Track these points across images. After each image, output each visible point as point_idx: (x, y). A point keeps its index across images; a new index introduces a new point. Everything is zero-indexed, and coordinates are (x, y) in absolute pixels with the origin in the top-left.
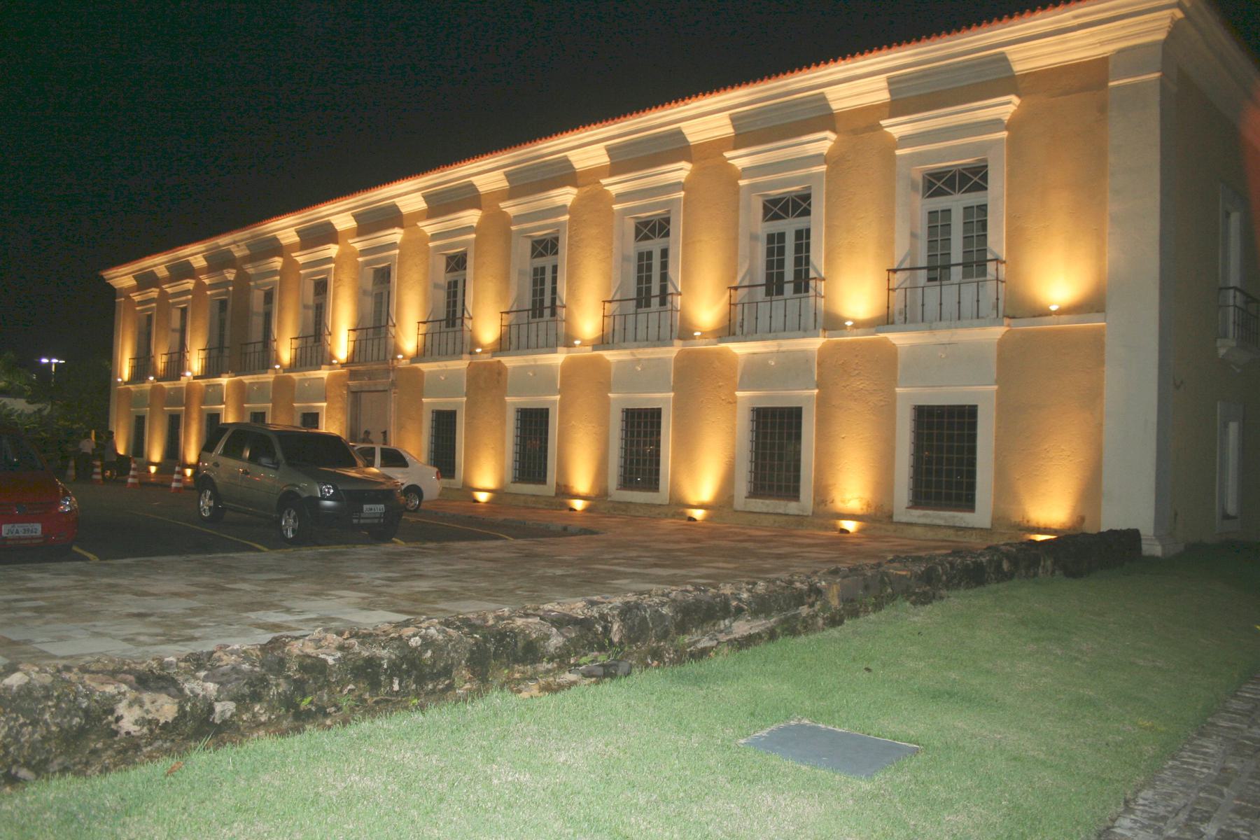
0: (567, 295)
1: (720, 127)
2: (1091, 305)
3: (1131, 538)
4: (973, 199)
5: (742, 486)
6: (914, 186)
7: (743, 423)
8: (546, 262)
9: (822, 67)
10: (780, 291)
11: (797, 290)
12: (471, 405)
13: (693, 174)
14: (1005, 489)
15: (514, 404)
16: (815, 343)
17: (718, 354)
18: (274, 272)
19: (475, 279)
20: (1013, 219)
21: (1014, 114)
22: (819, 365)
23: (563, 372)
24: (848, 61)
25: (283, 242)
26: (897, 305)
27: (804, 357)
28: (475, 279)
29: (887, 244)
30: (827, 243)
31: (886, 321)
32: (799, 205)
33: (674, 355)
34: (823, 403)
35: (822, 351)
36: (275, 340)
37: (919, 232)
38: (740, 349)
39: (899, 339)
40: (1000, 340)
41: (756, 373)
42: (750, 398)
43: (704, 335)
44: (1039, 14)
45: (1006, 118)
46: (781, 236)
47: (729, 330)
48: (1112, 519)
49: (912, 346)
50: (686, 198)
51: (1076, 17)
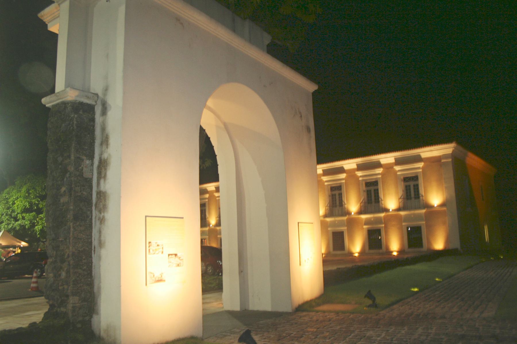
0: (346, 202)
1: (354, 166)
2: (442, 205)
3: (457, 249)
4: (376, 187)
5: (367, 247)
6: (402, 180)
7: (365, 233)
8: (203, 208)
9: (380, 155)
10: (411, 198)
11: (375, 202)
12: (209, 238)
13: (347, 176)
14: (429, 243)
15: (405, 225)
16: (382, 215)
17: (358, 218)
18: (206, 199)
19: (383, 189)
20: (425, 188)
21: (423, 166)
22: (384, 219)
23: (384, 218)
24: (331, 163)
25: (208, 190)
26: (363, 209)
27: (380, 218)
28: (383, 189)
29: (397, 193)
30: (383, 193)
31: (399, 209)
32: (415, 178)
33: (346, 219)
34: (386, 227)
35: (384, 216)
36: (208, 218)
37: (98, 223)
38: (364, 217)
39: (402, 213)
40: (425, 212)
41: (367, 222)
42: (368, 228)
43: (393, 210)
44: (325, 164)
45: (421, 167)
46: (409, 186)
47: (360, 212)
48: (451, 247)
49: (405, 215)
50: (345, 182)
51: (434, 148)
